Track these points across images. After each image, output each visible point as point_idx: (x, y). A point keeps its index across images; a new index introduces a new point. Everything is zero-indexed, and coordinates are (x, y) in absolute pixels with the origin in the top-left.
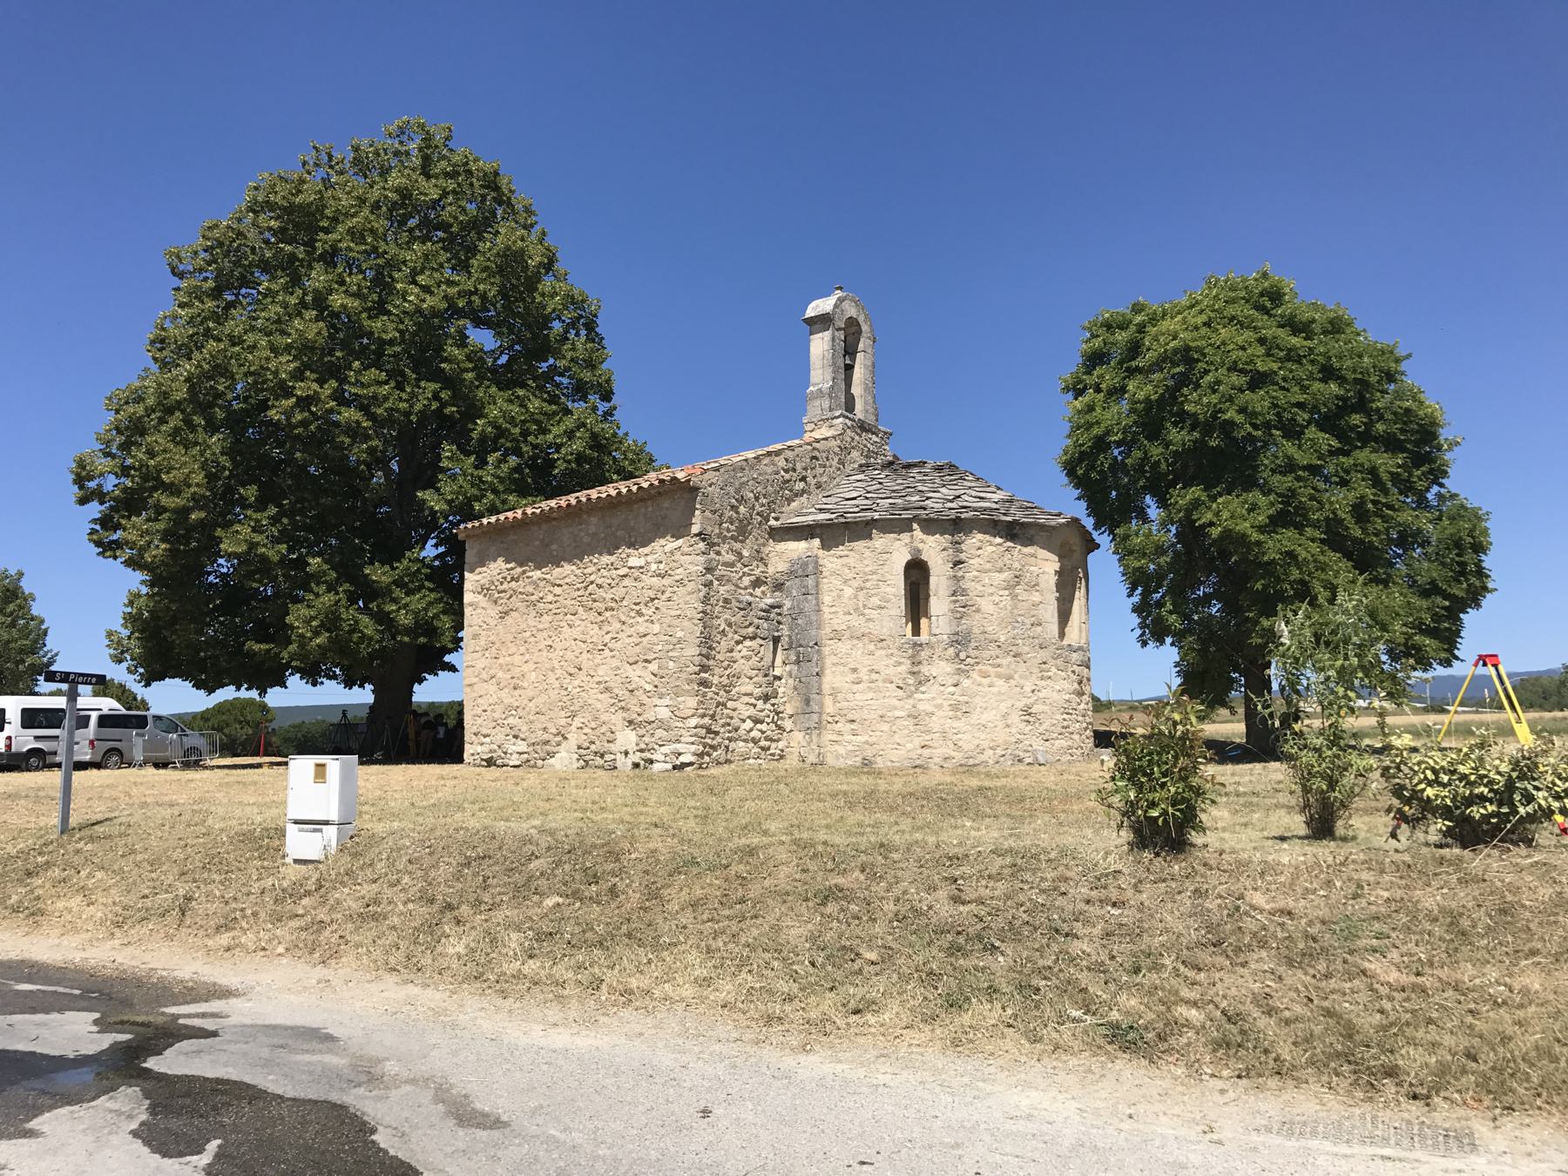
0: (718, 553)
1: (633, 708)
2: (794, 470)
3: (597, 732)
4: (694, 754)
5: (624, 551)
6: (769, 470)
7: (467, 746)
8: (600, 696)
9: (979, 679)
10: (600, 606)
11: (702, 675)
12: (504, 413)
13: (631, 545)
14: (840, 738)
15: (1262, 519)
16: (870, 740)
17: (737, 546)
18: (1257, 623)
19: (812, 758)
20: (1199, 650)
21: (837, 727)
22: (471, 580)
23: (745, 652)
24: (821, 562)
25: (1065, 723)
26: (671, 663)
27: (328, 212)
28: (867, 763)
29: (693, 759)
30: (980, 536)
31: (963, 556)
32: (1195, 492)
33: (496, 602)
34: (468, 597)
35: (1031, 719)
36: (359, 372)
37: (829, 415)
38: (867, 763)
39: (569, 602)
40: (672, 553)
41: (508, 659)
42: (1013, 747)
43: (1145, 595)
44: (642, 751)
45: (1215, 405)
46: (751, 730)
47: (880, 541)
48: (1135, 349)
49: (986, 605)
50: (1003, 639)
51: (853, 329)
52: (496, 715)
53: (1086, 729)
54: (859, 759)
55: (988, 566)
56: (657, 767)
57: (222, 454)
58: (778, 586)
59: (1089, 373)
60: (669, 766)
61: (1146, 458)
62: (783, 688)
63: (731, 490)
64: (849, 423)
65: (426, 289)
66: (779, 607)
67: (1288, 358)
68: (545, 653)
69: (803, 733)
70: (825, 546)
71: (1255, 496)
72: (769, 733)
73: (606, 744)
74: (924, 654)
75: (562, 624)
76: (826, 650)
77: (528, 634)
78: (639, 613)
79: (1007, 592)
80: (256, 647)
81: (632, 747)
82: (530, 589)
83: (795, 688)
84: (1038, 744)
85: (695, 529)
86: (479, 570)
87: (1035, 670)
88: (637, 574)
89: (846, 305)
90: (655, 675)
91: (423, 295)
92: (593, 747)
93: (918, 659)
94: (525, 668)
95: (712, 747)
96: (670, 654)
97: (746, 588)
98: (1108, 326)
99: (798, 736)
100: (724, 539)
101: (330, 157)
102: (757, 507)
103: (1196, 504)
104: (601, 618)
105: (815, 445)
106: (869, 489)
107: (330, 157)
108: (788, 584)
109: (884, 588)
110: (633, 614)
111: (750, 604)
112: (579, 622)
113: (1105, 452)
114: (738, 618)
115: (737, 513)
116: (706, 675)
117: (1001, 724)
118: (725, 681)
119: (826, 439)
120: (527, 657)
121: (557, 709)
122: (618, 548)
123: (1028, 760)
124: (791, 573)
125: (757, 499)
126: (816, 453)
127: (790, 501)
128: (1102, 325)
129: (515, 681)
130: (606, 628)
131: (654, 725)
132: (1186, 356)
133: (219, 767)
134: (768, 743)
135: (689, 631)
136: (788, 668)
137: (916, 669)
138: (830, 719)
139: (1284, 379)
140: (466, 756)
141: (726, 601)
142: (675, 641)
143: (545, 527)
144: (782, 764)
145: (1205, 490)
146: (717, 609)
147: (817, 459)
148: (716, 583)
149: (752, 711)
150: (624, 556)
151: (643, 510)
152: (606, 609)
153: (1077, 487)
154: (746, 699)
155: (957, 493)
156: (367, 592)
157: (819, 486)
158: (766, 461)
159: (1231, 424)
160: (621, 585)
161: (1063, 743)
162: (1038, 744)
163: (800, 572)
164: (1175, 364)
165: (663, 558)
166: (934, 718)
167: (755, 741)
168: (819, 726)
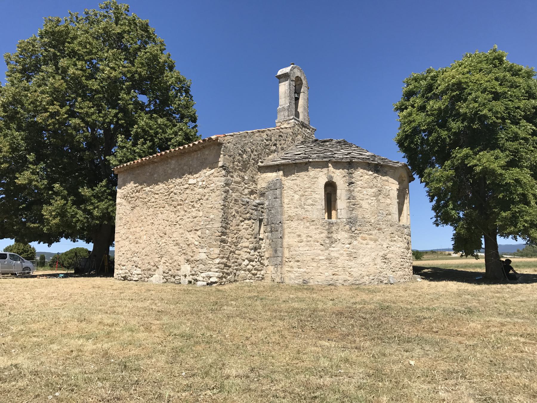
0: (232, 177)
1: (189, 253)
2: (271, 140)
3: (172, 265)
4: (218, 277)
5: (187, 176)
6: (259, 139)
7: (115, 270)
8: (174, 247)
9: (361, 241)
10: (175, 203)
11: (223, 237)
12: (147, 124)
13: (190, 173)
14: (291, 270)
15: (502, 162)
16: (307, 271)
17: (242, 174)
18: (499, 214)
19: (278, 280)
20: (466, 228)
21: (290, 264)
22: (120, 192)
23: (245, 226)
24: (283, 182)
25: (402, 263)
26: (207, 231)
27: (71, 35)
28: (305, 282)
29: (216, 280)
30: (361, 170)
31: (353, 180)
32: (466, 151)
33: (130, 202)
34: (118, 200)
35: (387, 261)
36: (80, 103)
37: (288, 118)
38: (305, 282)
39: (161, 202)
40: (209, 176)
41: (134, 229)
42: (378, 275)
43: (438, 201)
44: (193, 275)
45: (476, 108)
46: (248, 265)
47: (312, 172)
48: (430, 88)
49: (364, 204)
50: (373, 221)
51: (299, 83)
52: (128, 256)
53: (410, 266)
54: (301, 280)
55: (366, 185)
56: (199, 283)
57: (22, 139)
58: (262, 195)
59: (408, 100)
60: (205, 283)
61: (439, 137)
62: (264, 244)
63: (239, 146)
64: (297, 122)
65: (113, 69)
66: (262, 204)
67: (511, 87)
68: (150, 226)
69: (273, 267)
70: (285, 175)
71: (497, 152)
72: (256, 266)
73: (176, 271)
74: (334, 228)
75: (158, 212)
76: (285, 226)
77: (143, 217)
78: (193, 207)
79: (375, 198)
80: (32, 225)
81: (188, 273)
82: (144, 196)
83: (270, 244)
84: (390, 274)
85: (220, 164)
86: (123, 187)
87: (389, 237)
88: (192, 187)
89: (296, 70)
90: (200, 237)
91: (111, 71)
92: (170, 272)
93: (331, 230)
94: (141, 233)
95: (227, 274)
96: (207, 226)
97: (246, 195)
98: (416, 80)
99: (271, 268)
100: (235, 170)
101: (77, 18)
102: (252, 156)
103: (467, 156)
104: (176, 209)
105: (281, 130)
106: (306, 150)
107: (77, 18)
108: (267, 193)
109: (314, 195)
110: (190, 207)
111: (248, 202)
112: (166, 211)
113: (418, 134)
114: (242, 209)
115: (242, 157)
116: (225, 237)
117: (372, 264)
118: (235, 240)
119: (286, 128)
120: (142, 228)
121: (154, 254)
122: (184, 175)
123: (385, 282)
124: (268, 188)
125: (252, 152)
126: (281, 134)
127: (268, 154)
128: (413, 80)
129: (137, 240)
130: (178, 214)
131: (198, 262)
132: (459, 86)
133: (43, 275)
134: (256, 272)
135: (216, 215)
136: (266, 234)
137: (330, 236)
138: (287, 260)
139: (511, 96)
140: (115, 275)
141: (236, 200)
142: (209, 220)
143: (151, 166)
144: (264, 283)
145: (471, 149)
146: (231, 204)
147: (282, 136)
148: (231, 191)
149: (248, 256)
150: (187, 178)
151: (196, 156)
152: (178, 205)
153: (404, 152)
154: (245, 250)
155: (349, 152)
156: (80, 201)
157: (282, 149)
158: (257, 134)
159: (485, 117)
160: (185, 193)
161: (400, 273)
162: (390, 274)
163: (273, 187)
164: (453, 91)
165: (205, 179)
166: (339, 260)
167: (249, 271)
168: (281, 263)
